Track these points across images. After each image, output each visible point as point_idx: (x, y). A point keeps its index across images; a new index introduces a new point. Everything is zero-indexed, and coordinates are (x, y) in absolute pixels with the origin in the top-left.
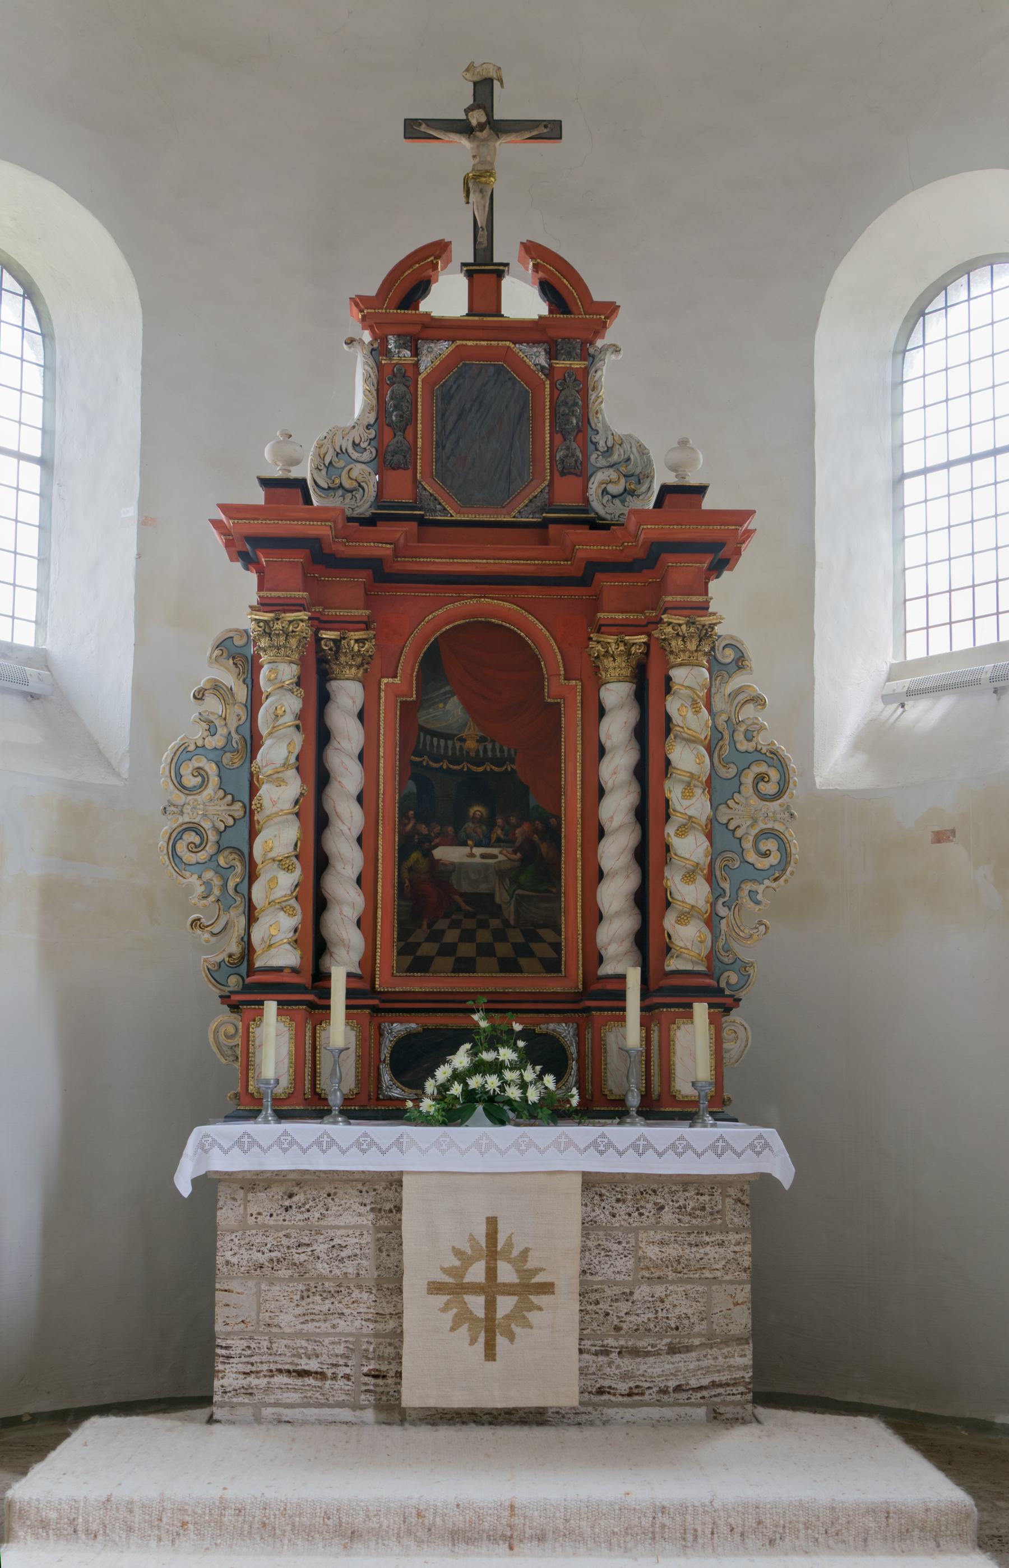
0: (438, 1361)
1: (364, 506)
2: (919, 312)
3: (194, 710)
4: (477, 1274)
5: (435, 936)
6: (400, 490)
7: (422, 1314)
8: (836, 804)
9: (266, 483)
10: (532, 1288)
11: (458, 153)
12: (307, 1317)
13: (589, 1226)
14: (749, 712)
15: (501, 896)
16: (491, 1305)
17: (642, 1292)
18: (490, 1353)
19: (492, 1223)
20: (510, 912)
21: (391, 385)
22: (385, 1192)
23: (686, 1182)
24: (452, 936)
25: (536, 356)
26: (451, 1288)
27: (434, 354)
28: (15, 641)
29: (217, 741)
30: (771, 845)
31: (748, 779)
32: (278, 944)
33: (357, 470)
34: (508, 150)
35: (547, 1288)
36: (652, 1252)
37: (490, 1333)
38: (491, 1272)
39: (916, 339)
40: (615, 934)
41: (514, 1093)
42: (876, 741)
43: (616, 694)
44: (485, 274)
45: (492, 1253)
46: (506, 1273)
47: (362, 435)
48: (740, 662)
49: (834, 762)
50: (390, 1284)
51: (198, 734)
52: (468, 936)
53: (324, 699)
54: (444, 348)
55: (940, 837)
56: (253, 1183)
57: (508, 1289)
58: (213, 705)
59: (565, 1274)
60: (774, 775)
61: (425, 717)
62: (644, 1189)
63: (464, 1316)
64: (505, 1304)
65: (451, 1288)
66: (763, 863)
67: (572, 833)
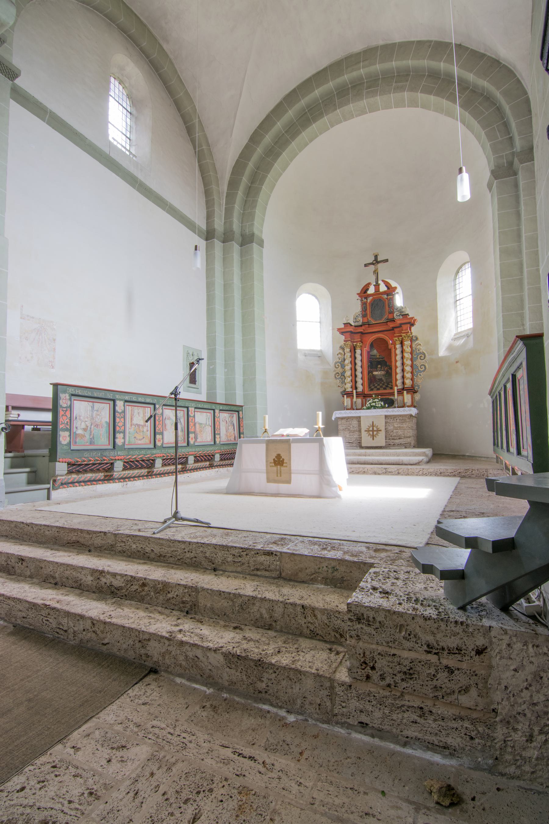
0: (366, 440)
1: (360, 323)
2: (458, 272)
3: (337, 357)
4: (371, 429)
5: (374, 385)
6: (366, 321)
7: (364, 434)
8: (442, 358)
9: (344, 324)
10: (378, 431)
11: (372, 267)
12: (350, 435)
13: (386, 423)
14: (418, 347)
15: (383, 379)
16: (373, 433)
17: (395, 431)
18: (373, 439)
19: (373, 422)
20: (385, 381)
21: (364, 305)
22: (359, 418)
23: (400, 416)
24: (376, 385)
25: (385, 296)
26: (368, 431)
27: (370, 299)
28: (471, 293)
29: (340, 361)
30: (423, 367)
31: (419, 357)
32: (348, 387)
33: (359, 318)
34: (380, 266)
35: (380, 430)
36: (396, 426)
37: (373, 436)
38: (373, 429)
39: (458, 277)
40: (399, 382)
41: (377, 405)
42: (450, 348)
43: (398, 346)
44: (377, 286)
45: (373, 426)
46: (375, 429)
47: (360, 313)
48: (417, 339)
49: (442, 352)
50: (360, 431)
51: (338, 360)
52: (379, 385)
53: (355, 352)
54: (371, 298)
55: (457, 362)
56: (342, 418)
57: (375, 431)
58: (340, 356)
59: (383, 428)
60: (423, 356)
61: (371, 353)
62: (394, 417)
63: (369, 434)
64: (375, 433)
65: (368, 431)
66: (421, 370)
67: (393, 368)
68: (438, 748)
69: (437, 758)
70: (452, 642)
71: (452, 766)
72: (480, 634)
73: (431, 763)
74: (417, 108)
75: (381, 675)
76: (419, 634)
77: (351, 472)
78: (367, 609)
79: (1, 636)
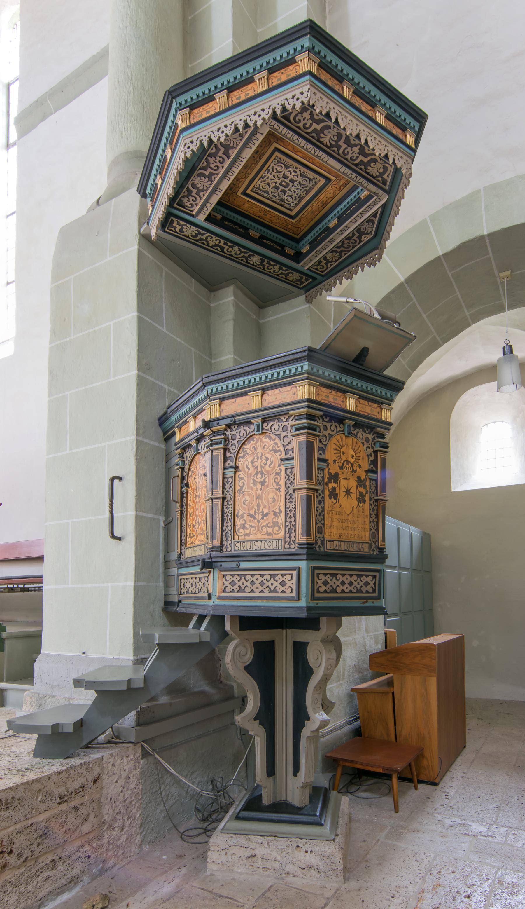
68: (66, 887)
69: (66, 897)
70: (77, 785)
71: (78, 892)
72: (97, 766)
73: (66, 903)
74: (47, 394)
75: (18, 855)
76: (54, 790)
77: (41, 577)
78: (6, 791)
79: (372, 906)
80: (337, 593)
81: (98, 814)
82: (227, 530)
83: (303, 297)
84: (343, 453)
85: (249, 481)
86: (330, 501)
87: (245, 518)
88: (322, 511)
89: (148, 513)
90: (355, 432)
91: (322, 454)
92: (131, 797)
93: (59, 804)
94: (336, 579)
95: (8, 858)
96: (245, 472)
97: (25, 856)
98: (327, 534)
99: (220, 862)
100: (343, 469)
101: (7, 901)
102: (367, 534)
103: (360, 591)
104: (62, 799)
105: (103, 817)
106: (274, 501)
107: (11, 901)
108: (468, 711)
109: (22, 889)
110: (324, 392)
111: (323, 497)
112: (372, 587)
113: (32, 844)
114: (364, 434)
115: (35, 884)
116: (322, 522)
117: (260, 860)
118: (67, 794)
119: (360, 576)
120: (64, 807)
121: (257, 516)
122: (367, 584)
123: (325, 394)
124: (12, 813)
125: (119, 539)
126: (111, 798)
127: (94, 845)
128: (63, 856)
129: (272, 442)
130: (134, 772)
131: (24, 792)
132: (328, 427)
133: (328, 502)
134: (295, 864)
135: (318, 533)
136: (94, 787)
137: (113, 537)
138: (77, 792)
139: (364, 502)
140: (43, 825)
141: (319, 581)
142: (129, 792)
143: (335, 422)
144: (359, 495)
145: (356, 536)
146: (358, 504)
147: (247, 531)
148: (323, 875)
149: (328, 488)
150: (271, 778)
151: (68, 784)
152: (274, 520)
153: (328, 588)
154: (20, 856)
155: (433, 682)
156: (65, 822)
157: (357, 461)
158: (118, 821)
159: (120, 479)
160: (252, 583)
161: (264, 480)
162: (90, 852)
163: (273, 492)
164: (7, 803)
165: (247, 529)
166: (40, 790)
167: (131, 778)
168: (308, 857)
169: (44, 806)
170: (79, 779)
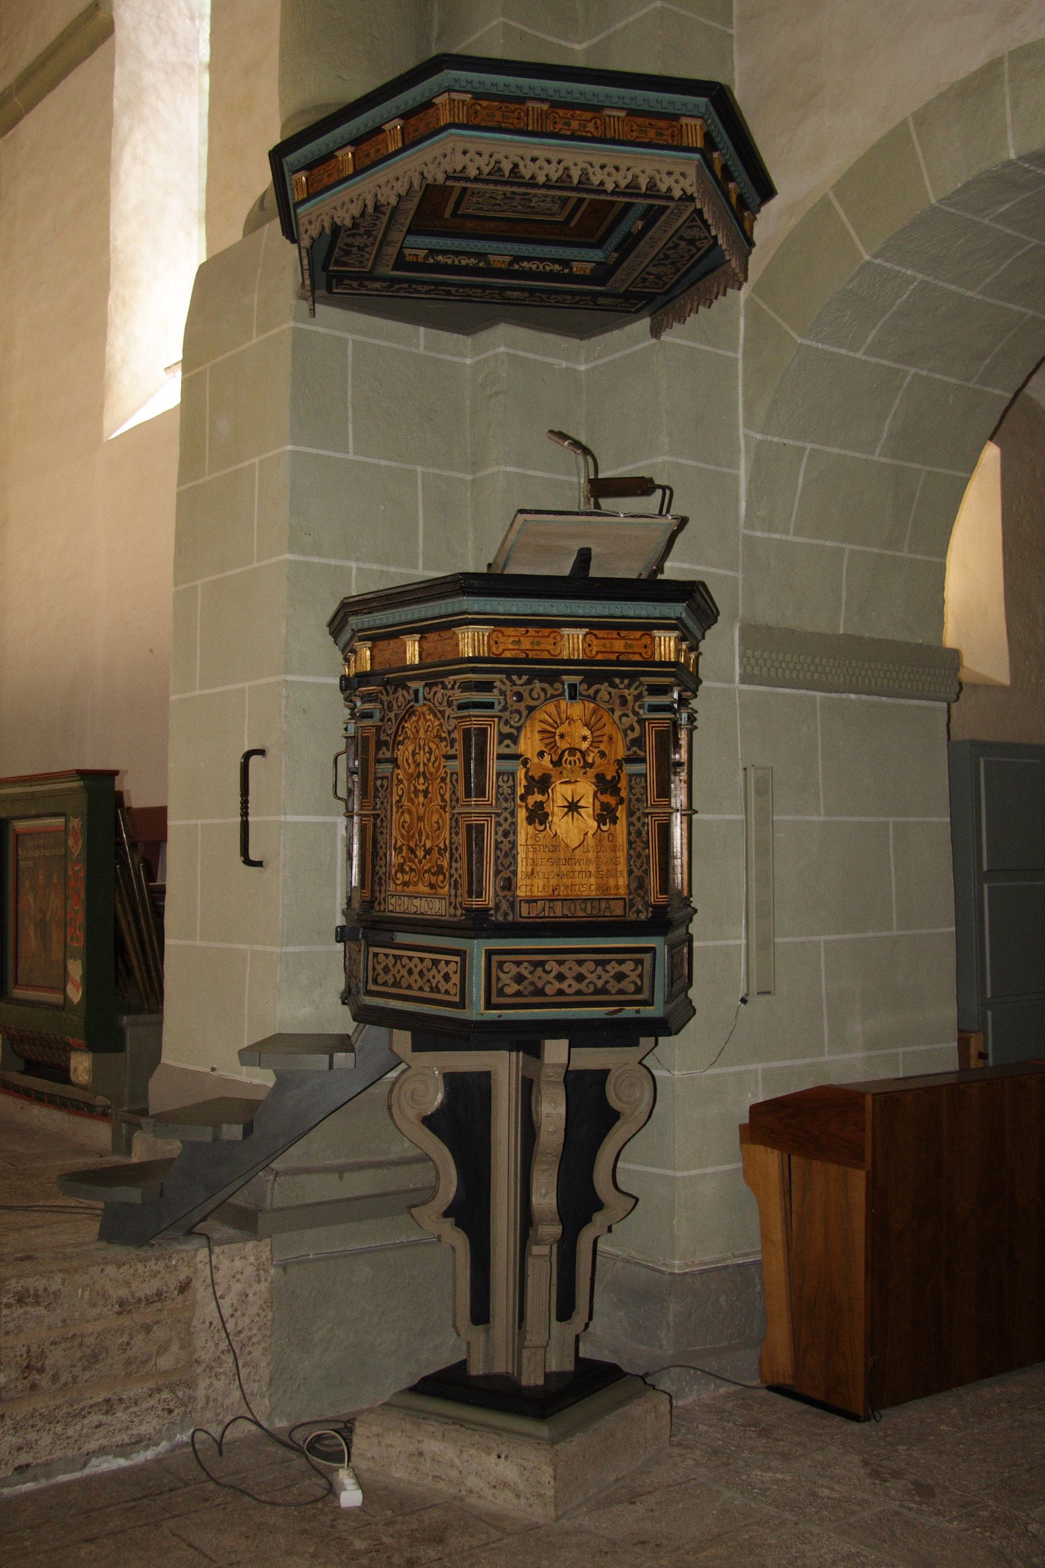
80: (546, 995)
81: (187, 1345)
82: (381, 873)
83: (646, 323)
84: (562, 736)
85: (409, 787)
86: (531, 828)
87: (404, 854)
88: (511, 849)
89: (309, 814)
90: (591, 691)
91: (512, 745)
92: (251, 1329)
93: (119, 1313)
94: (545, 971)
95: (37, 1377)
96: (405, 770)
97: (63, 1380)
98: (523, 889)
99: (369, 1455)
100: (561, 764)
101: (36, 1440)
102: (622, 881)
103: (603, 991)
104: (124, 1306)
105: (194, 1352)
106: (439, 828)
107: (42, 1443)
108: (557, 1217)
109: (59, 1429)
110: (509, 636)
111: (513, 823)
112: (635, 983)
113: (73, 1366)
114: (613, 691)
115: (79, 1427)
116: (512, 868)
117: (428, 1460)
118: (131, 1300)
119: (602, 963)
120: (125, 1321)
121: (418, 853)
122: (620, 977)
123: (511, 639)
124: (44, 1312)
125: (259, 864)
126: (211, 1323)
127: (180, 1394)
128: (124, 1397)
129: (437, 723)
130: (256, 1287)
131: (63, 1284)
132: (526, 695)
133: (524, 831)
134: (480, 1477)
135: (503, 888)
136: (179, 1299)
137: (248, 862)
138: (149, 1301)
139: (614, 820)
140: (91, 1341)
141: (502, 976)
142: (248, 1321)
143: (541, 681)
144: (601, 810)
145: (593, 887)
146: (599, 827)
147: (406, 878)
148: (523, 1501)
149: (527, 805)
150: (481, 1327)
151: (134, 1285)
152: (439, 862)
153: (613, 968)
154: (55, 1378)
155: (859, 1179)
156: (128, 1344)
157: (596, 744)
158: (225, 1365)
159: (261, 752)
160: (410, 972)
161: (427, 788)
162: (172, 1404)
163: (438, 812)
164: (37, 1296)
165: (407, 873)
166: (87, 1285)
167: (251, 1295)
168: (502, 1467)
169: (93, 1312)
170: (152, 1280)
